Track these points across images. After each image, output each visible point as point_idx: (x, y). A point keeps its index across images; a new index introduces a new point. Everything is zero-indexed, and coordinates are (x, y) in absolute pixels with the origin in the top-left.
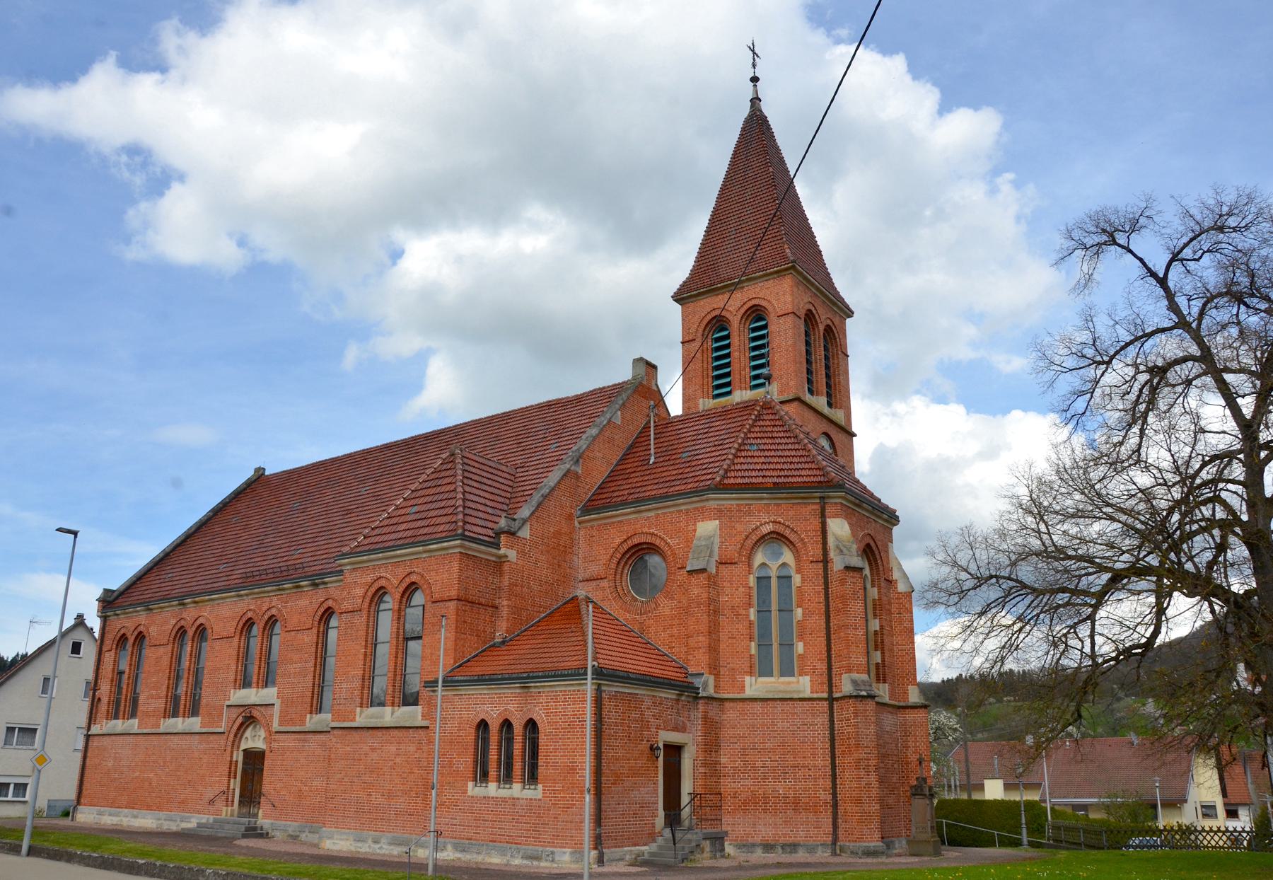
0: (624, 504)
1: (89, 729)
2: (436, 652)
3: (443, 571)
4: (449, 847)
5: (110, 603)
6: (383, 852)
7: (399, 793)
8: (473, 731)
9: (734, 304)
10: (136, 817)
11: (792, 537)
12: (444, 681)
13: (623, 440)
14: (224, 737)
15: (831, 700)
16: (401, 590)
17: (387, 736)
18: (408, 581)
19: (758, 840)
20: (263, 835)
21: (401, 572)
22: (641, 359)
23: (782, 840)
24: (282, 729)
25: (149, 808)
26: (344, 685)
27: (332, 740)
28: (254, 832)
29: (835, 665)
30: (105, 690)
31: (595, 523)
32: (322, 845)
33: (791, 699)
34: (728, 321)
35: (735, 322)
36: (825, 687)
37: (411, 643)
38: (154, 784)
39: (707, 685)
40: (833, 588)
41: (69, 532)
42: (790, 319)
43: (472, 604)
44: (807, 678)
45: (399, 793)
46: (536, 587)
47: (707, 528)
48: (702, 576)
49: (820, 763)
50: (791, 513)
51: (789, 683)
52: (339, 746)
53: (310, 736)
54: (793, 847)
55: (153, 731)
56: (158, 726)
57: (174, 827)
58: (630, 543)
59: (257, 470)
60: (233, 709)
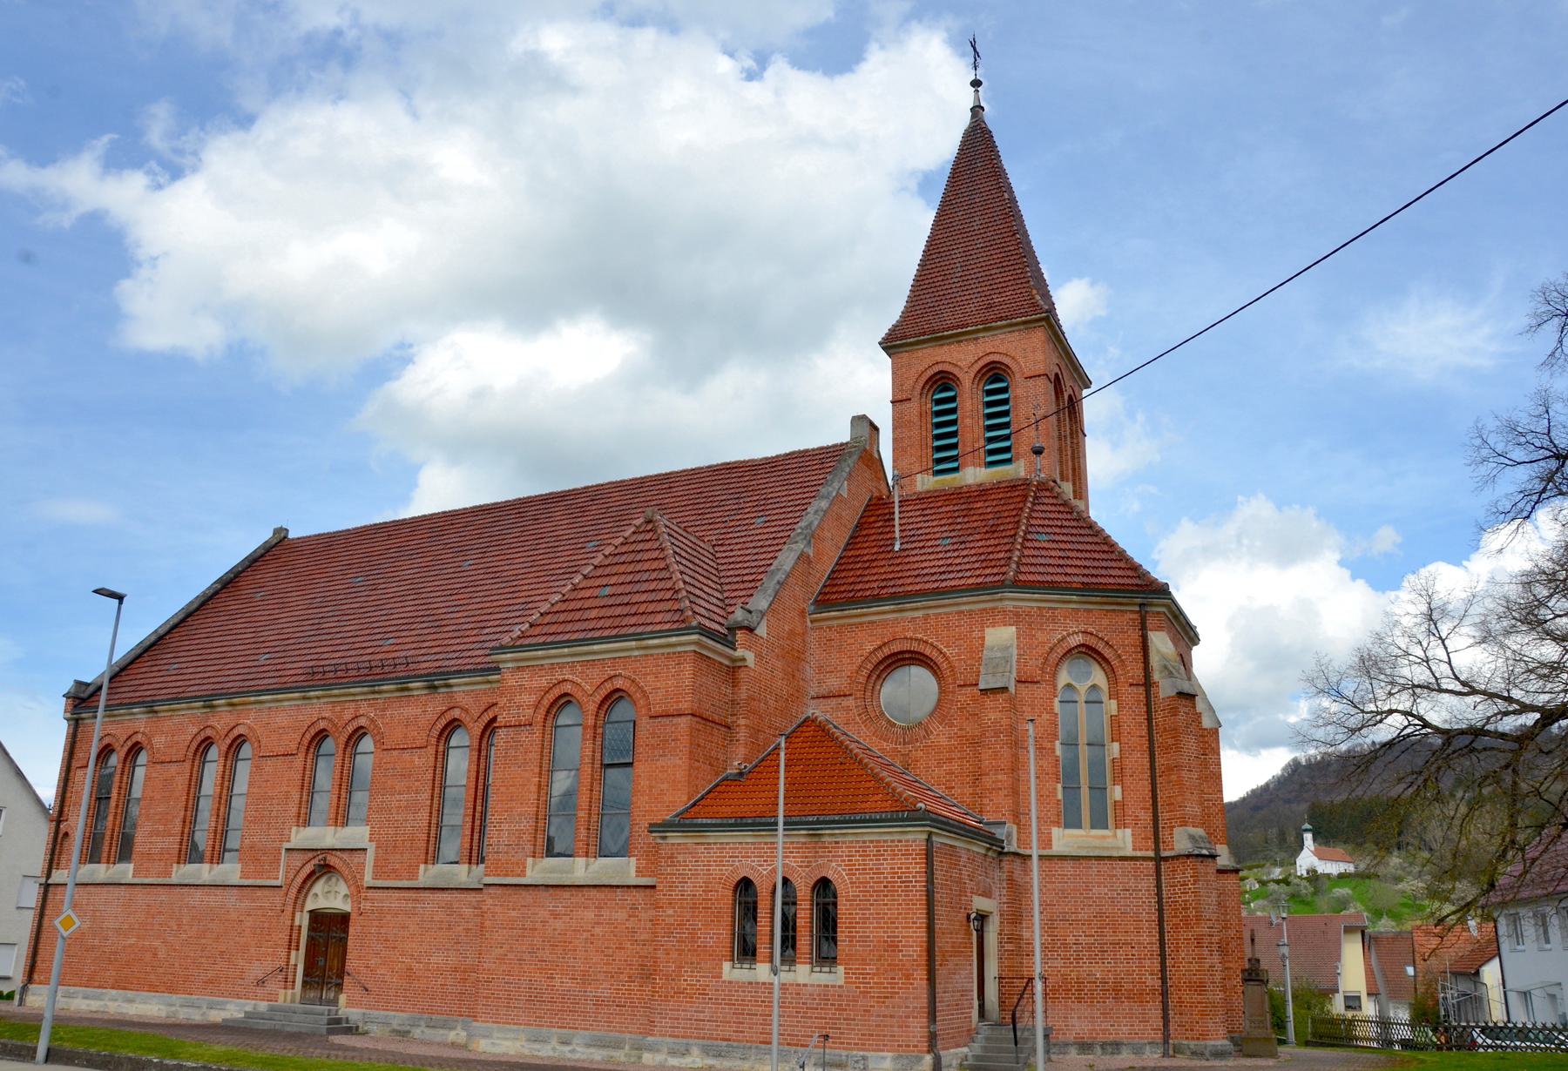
0: (877, 599)
1: (49, 876)
2: (664, 779)
3: (665, 673)
4: (695, 1051)
5: (83, 700)
6: (577, 1056)
7: (601, 977)
8: (730, 893)
9: (963, 358)
10: (131, 1001)
11: (1107, 652)
12: (785, 824)
13: (851, 517)
14: (282, 892)
15: (1159, 860)
16: (598, 698)
17: (579, 897)
18: (609, 687)
19: (1071, 1037)
20: (351, 1030)
21: (597, 675)
22: (864, 417)
23: (1101, 1038)
24: (379, 883)
25: (153, 988)
26: (505, 827)
27: (488, 900)
28: (338, 1026)
29: (1163, 816)
30: (78, 824)
31: (835, 622)
32: (472, 1046)
33: (1110, 858)
34: (955, 378)
35: (966, 380)
36: (1151, 843)
37: (610, 771)
38: (161, 955)
39: (1008, 833)
40: (1159, 718)
41: (113, 595)
42: (1042, 381)
43: (712, 723)
44: (1128, 831)
45: (601, 977)
46: (771, 702)
47: (1001, 636)
48: (1001, 697)
49: (1145, 939)
50: (1105, 622)
51: (1104, 837)
52: (498, 909)
53: (427, 894)
54: (1116, 1046)
55: (160, 881)
56: (169, 874)
57: (196, 1016)
58: (887, 651)
59: (277, 531)
60: (295, 854)
